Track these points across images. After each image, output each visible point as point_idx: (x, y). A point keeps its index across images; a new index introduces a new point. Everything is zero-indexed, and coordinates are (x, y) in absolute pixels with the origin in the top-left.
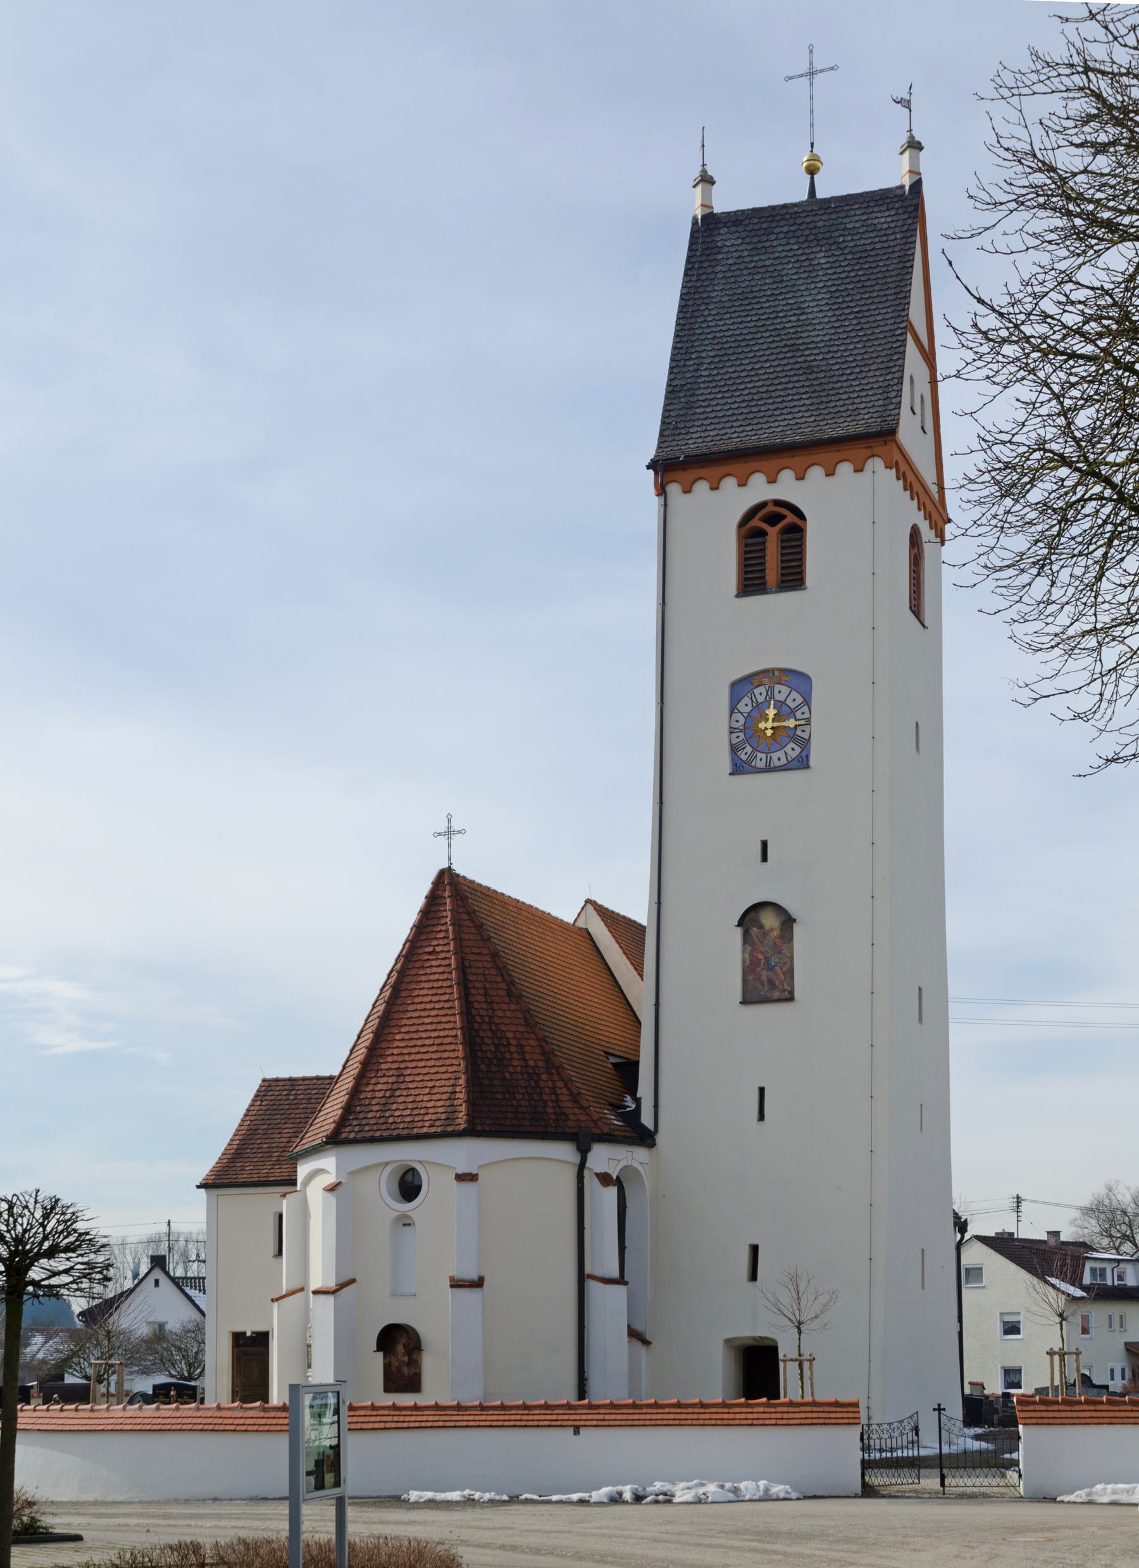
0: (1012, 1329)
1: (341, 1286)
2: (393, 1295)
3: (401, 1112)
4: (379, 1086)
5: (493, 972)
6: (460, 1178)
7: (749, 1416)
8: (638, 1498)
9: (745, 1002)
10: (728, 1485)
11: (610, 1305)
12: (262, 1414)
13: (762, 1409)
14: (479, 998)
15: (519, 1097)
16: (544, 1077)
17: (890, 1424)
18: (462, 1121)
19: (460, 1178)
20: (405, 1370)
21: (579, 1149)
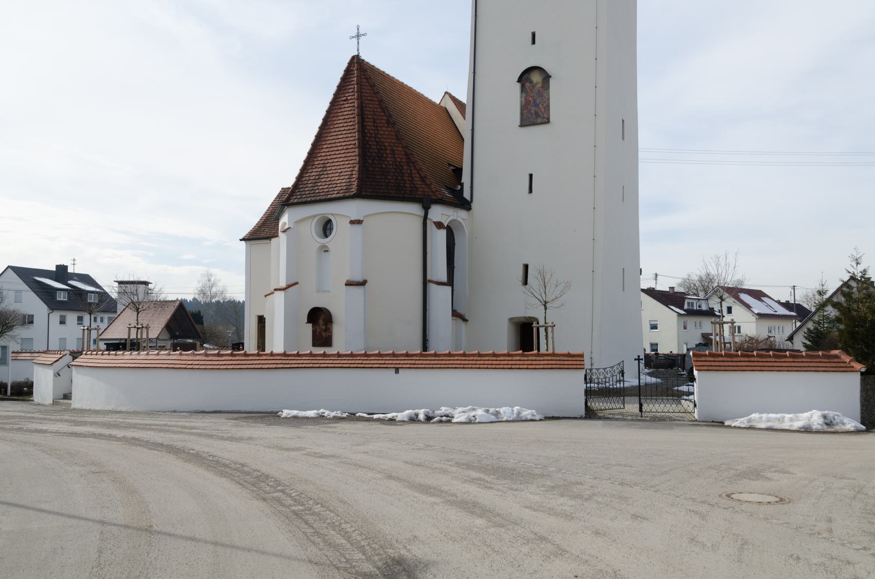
0: (654, 327)
1: (289, 286)
2: (318, 291)
3: (323, 186)
4: (313, 173)
5: (379, 110)
6: (352, 222)
7: (510, 362)
8: (429, 419)
9: (522, 126)
10: (492, 410)
11: (441, 297)
12: (204, 358)
13: (518, 358)
14: (370, 124)
15: (389, 177)
16: (405, 167)
17: (605, 369)
18: (354, 189)
19: (352, 222)
20: (324, 334)
21: (423, 207)
